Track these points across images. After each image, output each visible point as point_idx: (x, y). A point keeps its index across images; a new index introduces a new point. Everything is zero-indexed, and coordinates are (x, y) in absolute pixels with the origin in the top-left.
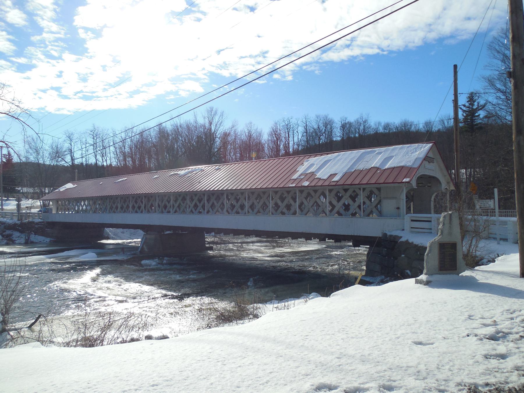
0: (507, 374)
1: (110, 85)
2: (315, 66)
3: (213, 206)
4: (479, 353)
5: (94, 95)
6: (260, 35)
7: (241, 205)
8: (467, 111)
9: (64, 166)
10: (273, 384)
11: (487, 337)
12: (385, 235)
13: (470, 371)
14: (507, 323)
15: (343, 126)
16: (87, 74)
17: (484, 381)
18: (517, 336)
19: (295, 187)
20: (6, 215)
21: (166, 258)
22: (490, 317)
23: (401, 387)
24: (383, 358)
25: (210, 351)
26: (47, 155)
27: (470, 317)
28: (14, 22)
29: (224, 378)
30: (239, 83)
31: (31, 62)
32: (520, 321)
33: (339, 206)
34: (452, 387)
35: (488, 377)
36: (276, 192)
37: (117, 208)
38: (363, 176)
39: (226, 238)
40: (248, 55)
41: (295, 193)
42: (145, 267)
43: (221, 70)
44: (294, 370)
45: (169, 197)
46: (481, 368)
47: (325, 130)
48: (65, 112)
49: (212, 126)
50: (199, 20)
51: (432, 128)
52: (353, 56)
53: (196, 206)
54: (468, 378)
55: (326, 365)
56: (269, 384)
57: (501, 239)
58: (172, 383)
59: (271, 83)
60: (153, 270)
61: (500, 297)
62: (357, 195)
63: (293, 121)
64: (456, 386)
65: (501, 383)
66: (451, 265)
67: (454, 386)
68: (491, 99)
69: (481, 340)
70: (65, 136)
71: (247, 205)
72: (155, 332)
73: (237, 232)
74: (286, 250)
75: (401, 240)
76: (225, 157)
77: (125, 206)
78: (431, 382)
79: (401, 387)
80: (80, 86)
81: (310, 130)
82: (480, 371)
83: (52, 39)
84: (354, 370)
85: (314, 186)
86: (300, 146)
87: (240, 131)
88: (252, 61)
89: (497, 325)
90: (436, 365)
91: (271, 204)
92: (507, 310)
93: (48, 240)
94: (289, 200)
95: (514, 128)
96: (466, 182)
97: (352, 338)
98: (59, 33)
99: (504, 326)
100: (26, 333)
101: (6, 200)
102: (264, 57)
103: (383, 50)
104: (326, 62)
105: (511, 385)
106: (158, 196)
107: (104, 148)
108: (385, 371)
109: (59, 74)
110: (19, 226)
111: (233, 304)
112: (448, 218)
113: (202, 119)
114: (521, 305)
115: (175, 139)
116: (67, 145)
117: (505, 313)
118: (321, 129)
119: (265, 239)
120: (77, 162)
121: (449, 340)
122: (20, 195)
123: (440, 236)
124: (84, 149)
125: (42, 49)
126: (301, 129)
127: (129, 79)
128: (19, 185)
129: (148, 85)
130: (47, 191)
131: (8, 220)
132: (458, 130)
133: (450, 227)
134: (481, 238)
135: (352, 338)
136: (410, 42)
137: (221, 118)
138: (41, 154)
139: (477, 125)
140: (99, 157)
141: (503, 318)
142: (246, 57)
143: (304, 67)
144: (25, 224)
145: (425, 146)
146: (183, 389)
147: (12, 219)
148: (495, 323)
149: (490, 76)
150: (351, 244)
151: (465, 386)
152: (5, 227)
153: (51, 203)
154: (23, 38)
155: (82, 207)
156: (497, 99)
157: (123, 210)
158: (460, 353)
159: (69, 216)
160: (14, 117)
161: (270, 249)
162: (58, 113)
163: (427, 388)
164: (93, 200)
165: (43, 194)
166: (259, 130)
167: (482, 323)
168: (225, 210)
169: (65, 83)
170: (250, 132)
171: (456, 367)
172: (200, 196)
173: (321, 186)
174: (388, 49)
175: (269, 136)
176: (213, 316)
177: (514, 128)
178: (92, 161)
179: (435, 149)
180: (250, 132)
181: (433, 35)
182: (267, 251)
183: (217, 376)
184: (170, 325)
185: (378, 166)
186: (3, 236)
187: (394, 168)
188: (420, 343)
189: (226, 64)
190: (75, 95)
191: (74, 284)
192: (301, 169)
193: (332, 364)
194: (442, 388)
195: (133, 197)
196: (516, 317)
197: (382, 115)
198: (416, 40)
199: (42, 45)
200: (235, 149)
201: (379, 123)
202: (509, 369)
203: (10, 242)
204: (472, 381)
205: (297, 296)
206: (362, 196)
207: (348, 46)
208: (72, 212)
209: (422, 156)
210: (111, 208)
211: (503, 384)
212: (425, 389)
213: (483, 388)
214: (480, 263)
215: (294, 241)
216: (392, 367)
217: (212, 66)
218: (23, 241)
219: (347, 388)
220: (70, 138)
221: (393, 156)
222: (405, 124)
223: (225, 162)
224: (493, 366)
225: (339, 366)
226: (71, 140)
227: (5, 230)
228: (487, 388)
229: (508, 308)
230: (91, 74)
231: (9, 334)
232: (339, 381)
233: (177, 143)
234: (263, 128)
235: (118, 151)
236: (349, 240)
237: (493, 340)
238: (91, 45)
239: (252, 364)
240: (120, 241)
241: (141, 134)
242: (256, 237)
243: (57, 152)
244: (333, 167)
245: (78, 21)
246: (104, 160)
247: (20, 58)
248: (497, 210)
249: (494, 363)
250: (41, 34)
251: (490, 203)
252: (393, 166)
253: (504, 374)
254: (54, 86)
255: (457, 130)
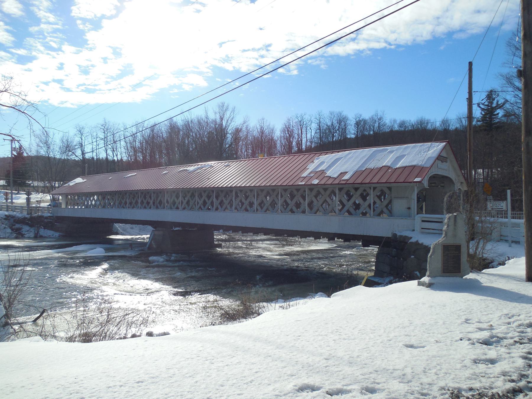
0: (493, 380)
1: (112, 77)
2: (321, 61)
3: (221, 203)
4: (469, 357)
5: (97, 88)
6: (262, 27)
7: (297, 202)
8: (486, 110)
9: (75, 160)
10: (257, 383)
11: (481, 341)
12: (395, 235)
13: (456, 375)
14: (503, 327)
15: (358, 124)
16: (88, 67)
17: (468, 386)
18: (512, 341)
19: (304, 185)
20: (16, 209)
21: (174, 255)
22: (487, 321)
23: (384, 390)
24: (371, 360)
25: (201, 349)
26: (58, 149)
27: (467, 321)
28: (11, 12)
29: (209, 376)
30: (247, 79)
31: (31, 54)
32: (517, 326)
33: (349, 205)
34: (435, 391)
35: (474, 381)
36: (285, 190)
37: (126, 203)
38: (374, 174)
39: (237, 236)
40: (251, 48)
41: (305, 191)
42: (154, 264)
43: (224, 63)
44: (281, 370)
45: (178, 194)
46: (467, 373)
47: (339, 127)
48: (68, 105)
49: (223, 121)
50: (198, 11)
51: (449, 126)
52: (359, 50)
53: (205, 203)
54: (453, 382)
55: (312, 366)
56: (253, 383)
57: (513, 242)
58: (158, 380)
59: (276, 77)
60: (158, 266)
61: (501, 301)
62: (368, 195)
63: (307, 117)
64: (439, 390)
65: (485, 388)
66: (455, 268)
67: (437, 390)
68: (508, 98)
69: (473, 344)
70: (76, 130)
71: (256, 203)
72: (156, 330)
73: (245, 230)
74: (296, 248)
75: (411, 241)
76: (236, 153)
77: (134, 202)
78: (415, 386)
79: (384, 390)
80: (82, 79)
81: (323, 127)
82: (467, 375)
83: (50, 30)
84: (340, 371)
85: (324, 184)
86: (313, 143)
87: (252, 127)
88: (255, 54)
89: (493, 329)
90: (423, 369)
91: (280, 202)
92: (506, 315)
93: (57, 234)
94: (298, 198)
95: (523, 129)
96: (484, 182)
97: (344, 339)
98: (57, 24)
99: (499, 331)
100: (29, 327)
101: (17, 194)
102: (268, 50)
103: (390, 44)
104: (332, 56)
105: (494, 391)
106: (167, 192)
107: (115, 142)
108: (371, 373)
109: (60, 66)
110: (29, 220)
111: (238, 303)
112: (452, 220)
113: (209, 112)
114: (521, 310)
115: (186, 134)
116: (77, 139)
117: (502, 318)
118: (335, 126)
119: (274, 238)
120: (87, 156)
121: (441, 344)
122: (31, 189)
123: (444, 237)
124: (95, 144)
125: (41, 40)
126: (314, 126)
127: (131, 72)
128: (29, 179)
129: (150, 78)
130: (57, 185)
131: (17, 214)
132: (472, 128)
133: (455, 229)
134: (490, 240)
135: (344, 339)
136: (418, 36)
137: (232, 113)
138: (52, 148)
139: (494, 124)
140: (110, 152)
141: (500, 322)
142: (248, 50)
143: (309, 61)
144: (34, 218)
145: (438, 145)
146: (168, 386)
147: (21, 213)
148: (491, 328)
149: (509, 73)
150: (361, 244)
151: (449, 390)
152: (14, 221)
153: (60, 197)
154: (21, 28)
155: (92, 201)
156: (515, 97)
157: (132, 206)
158: (450, 357)
159: (79, 211)
160: (20, 111)
161: (279, 247)
162: (62, 106)
163: (409, 391)
164: (103, 195)
165: (53, 188)
166: (271, 126)
167: (478, 327)
168: (234, 207)
169: (67, 76)
170: (262, 128)
171: (443, 371)
172: (209, 193)
173: (331, 184)
174: (395, 43)
175: (281, 133)
176: (218, 314)
177: (523, 129)
178: (103, 155)
179: (448, 147)
180: (262, 128)
181: (441, 29)
182: (277, 249)
183: (203, 375)
184: (174, 322)
185: (389, 164)
186: (12, 230)
187: (406, 167)
188: (412, 346)
189: (229, 57)
190: (78, 88)
191: (80, 279)
192: (311, 167)
193: (319, 365)
194: (425, 391)
195: (142, 193)
196: (514, 322)
197: (398, 113)
198: (425, 34)
199: (41, 36)
200: (247, 145)
201: (395, 121)
202: (496, 375)
203: (19, 235)
204: (456, 385)
205: (304, 295)
206: (372, 195)
207: (353, 40)
208: (81, 207)
209: (435, 155)
210: (120, 203)
211: (487, 389)
212: (407, 393)
213: (467, 392)
214: (490, 265)
215: (303, 239)
216: (378, 369)
217: (215, 59)
218: (32, 235)
219: (329, 389)
220: (81, 132)
221: (404, 156)
222: (421, 122)
223: (236, 159)
224: (480, 371)
225: (326, 367)
226: (82, 134)
227: (14, 223)
228: (471, 393)
229: (506, 313)
230: (93, 66)
231: (12, 328)
232: (323, 383)
233: (188, 139)
234: (276, 125)
235: (129, 146)
236: (359, 240)
237: (486, 344)
238: (91, 36)
239: (239, 363)
240: (129, 237)
241: (152, 128)
242: (265, 235)
243: (68, 146)
244: (344, 165)
245: (75, 11)
246: (115, 155)
247: (19, 49)
248: (509, 212)
249: (482, 367)
250: (39, 25)
251: (502, 205)
252: (404, 165)
253: (490, 379)
254: (56, 78)
255: (470, 129)
